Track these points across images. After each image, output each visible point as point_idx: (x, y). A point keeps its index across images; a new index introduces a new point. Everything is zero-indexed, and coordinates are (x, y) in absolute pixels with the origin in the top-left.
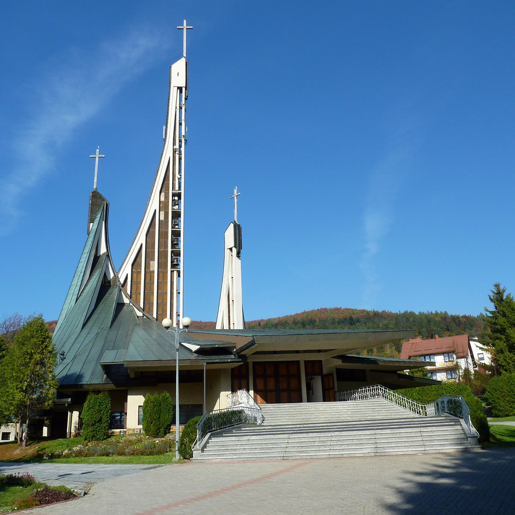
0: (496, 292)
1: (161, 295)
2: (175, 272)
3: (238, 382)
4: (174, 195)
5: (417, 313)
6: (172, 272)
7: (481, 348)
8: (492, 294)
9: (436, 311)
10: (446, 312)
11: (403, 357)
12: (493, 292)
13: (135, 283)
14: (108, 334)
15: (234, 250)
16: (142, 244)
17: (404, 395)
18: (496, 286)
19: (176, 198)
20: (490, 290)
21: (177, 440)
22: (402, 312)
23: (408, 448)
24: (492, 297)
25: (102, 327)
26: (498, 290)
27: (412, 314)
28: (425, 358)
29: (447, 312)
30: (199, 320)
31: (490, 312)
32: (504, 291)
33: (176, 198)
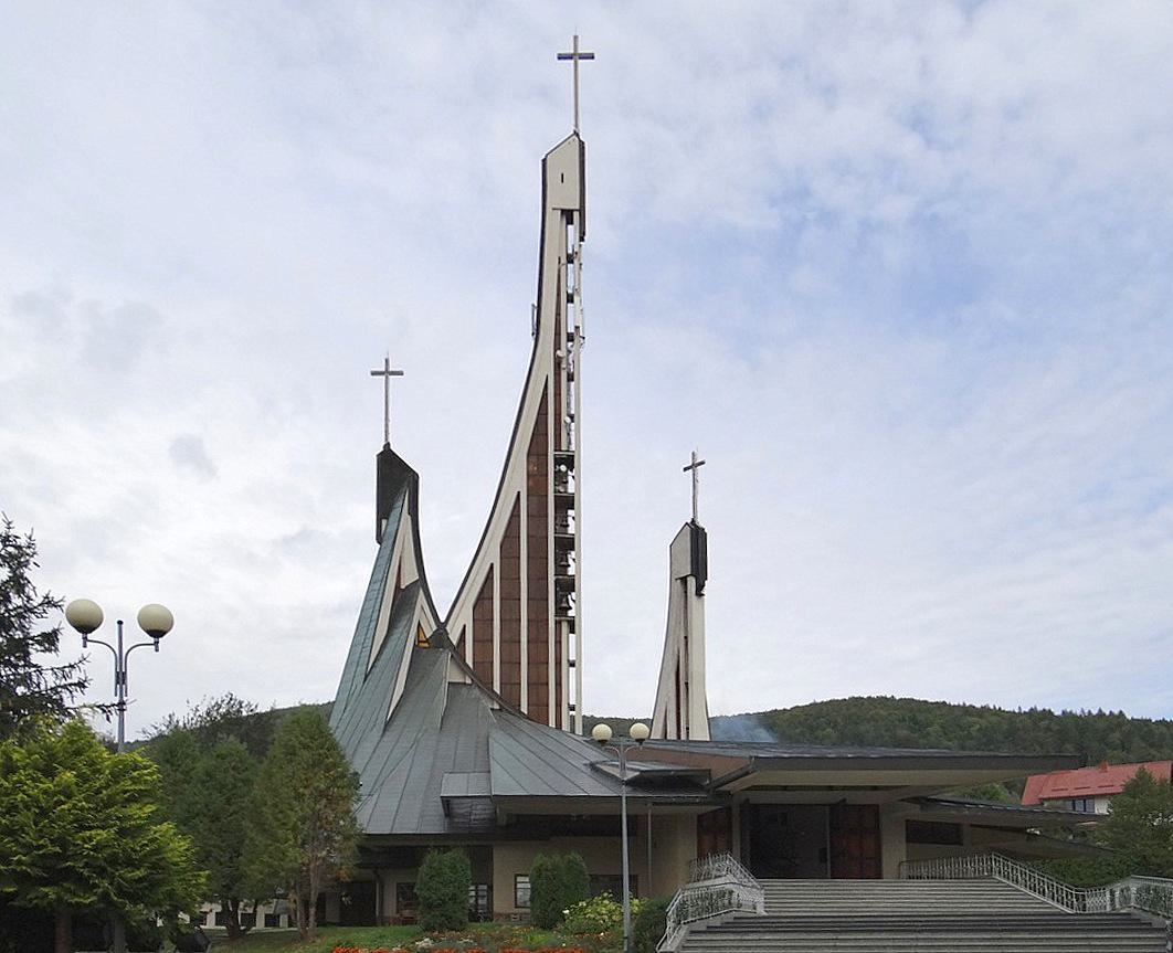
4: (558, 461)
5: (1058, 713)
9: (1100, 710)
11: (1028, 799)
13: (483, 641)
14: (438, 741)
15: (692, 582)
16: (492, 565)
19: (563, 468)
25: (424, 727)
27: (1047, 714)
28: (1074, 803)
29: (1125, 712)
33: (563, 468)
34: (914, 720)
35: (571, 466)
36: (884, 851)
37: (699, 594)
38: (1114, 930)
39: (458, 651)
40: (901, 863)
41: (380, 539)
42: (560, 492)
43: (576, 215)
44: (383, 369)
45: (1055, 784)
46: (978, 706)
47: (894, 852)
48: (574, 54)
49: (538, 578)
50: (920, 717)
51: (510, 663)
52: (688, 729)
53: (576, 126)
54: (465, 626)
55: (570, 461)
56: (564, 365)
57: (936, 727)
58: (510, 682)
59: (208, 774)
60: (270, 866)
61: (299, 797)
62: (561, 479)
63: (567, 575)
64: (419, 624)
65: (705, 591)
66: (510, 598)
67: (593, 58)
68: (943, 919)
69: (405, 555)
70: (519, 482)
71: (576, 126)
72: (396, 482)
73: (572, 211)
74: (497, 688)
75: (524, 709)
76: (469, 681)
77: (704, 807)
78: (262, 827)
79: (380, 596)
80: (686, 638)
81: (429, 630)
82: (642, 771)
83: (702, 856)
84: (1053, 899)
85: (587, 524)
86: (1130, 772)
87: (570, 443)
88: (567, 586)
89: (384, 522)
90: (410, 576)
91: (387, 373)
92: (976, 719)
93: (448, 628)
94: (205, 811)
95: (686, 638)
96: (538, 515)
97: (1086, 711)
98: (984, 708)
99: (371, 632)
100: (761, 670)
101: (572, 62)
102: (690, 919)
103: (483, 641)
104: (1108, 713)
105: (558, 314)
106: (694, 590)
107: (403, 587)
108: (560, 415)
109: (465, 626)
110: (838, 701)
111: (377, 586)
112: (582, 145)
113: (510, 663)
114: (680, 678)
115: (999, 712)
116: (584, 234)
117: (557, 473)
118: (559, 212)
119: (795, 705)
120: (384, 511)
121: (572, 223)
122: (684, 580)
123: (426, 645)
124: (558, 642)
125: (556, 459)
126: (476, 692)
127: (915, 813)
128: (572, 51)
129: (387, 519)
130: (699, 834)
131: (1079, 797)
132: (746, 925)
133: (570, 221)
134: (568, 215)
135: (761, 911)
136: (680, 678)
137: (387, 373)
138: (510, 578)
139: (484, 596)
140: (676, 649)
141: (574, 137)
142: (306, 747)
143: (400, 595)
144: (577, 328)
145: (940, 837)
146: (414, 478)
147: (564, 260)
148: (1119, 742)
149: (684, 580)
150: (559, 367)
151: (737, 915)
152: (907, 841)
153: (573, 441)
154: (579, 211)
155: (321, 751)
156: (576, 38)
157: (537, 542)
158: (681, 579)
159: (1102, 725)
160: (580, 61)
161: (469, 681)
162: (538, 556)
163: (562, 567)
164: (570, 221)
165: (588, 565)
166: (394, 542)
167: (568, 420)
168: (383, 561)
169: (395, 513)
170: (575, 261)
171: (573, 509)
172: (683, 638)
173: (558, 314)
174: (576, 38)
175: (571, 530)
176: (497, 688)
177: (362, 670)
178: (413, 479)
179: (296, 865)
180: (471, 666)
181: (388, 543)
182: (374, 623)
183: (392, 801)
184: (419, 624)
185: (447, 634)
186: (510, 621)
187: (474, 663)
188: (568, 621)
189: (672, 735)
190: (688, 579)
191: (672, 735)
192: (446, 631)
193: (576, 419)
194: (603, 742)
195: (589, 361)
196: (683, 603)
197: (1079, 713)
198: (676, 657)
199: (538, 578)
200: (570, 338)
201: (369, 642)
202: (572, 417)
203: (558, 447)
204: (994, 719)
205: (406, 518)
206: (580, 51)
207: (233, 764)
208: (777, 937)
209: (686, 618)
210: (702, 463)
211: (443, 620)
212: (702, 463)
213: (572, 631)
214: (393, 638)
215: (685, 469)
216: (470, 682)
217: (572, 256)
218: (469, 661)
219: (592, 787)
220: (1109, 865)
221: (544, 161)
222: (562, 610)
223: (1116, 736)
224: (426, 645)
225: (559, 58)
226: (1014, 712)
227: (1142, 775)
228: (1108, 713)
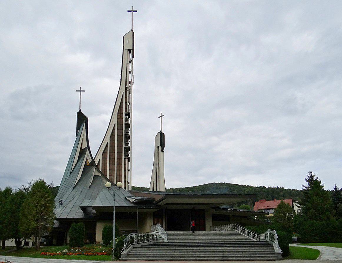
0: (309, 176)
2: (127, 160)
3: (157, 218)
4: (126, 115)
5: (267, 187)
7: (298, 207)
8: (307, 178)
9: (278, 187)
10: (283, 187)
11: (255, 209)
12: (308, 176)
13: (104, 164)
15: (160, 148)
16: (107, 143)
17: (248, 229)
18: (310, 172)
19: (127, 117)
20: (306, 175)
21: (113, 248)
22: (259, 186)
23: (241, 257)
24: (307, 179)
25: (85, 188)
26: (311, 174)
27: (264, 187)
28: (267, 210)
30: (146, 187)
31: (306, 187)
32: (314, 176)
34: (230, 189)
35: (129, 117)
36: (206, 223)
37: (162, 151)
38: (266, 246)
39: (97, 167)
41: (77, 135)
42: (126, 123)
43: (132, 51)
44: (80, 90)
45: (262, 205)
46: (247, 185)
47: (209, 224)
49: (120, 146)
50: (232, 188)
51: (112, 170)
52: (159, 189)
53: (132, 28)
55: (129, 115)
56: (128, 90)
57: (236, 191)
59: (12, 200)
60: (26, 227)
61: (36, 207)
62: (127, 120)
63: (128, 146)
64: (87, 159)
65: (164, 150)
66: (112, 152)
67: (137, 12)
68: (215, 243)
69: (84, 140)
70: (115, 121)
71: (132, 28)
72: (82, 120)
73: (131, 50)
77: (155, 210)
78: (24, 215)
79: (76, 151)
80: (159, 163)
81: (90, 160)
82: (135, 199)
83: (154, 224)
84: (254, 238)
85: (134, 133)
86: (279, 202)
87: (129, 110)
88: (128, 149)
89: (78, 131)
90: (85, 146)
91: (81, 91)
92: (246, 189)
93: (95, 160)
94: (10, 211)
95: (159, 163)
96: (120, 129)
97: (274, 187)
98: (248, 186)
99: (73, 161)
101: (131, 12)
102: (134, 243)
103: (104, 164)
104: (280, 187)
105: (126, 76)
106: (161, 150)
107: (83, 149)
108: (127, 103)
110: (210, 184)
111: (75, 148)
112: (133, 34)
114: (157, 175)
115: (252, 187)
116: (134, 56)
117: (126, 118)
120: (78, 128)
121: (130, 53)
122: (158, 147)
123: (89, 165)
124: (125, 164)
125: (125, 114)
126: (102, 178)
127: (214, 211)
128: (131, 10)
129: (79, 130)
130: (153, 218)
131: (268, 209)
132: (161, 245)
133: (130, 53)
134: (129, 51)
135: (166, 240)
136: (157, 175)
138: (112, 147)
139: (105, 152)
141: (131, 31)
142: (38, 191)
143: (83, 151)
144: (131, 80)
145: (222, 219)
146: (87, 119)
147: (128, 62)
148: (282, 195)
149: (158, 147)
150: (127, 89)
151: (155, 242)
153: (130, 110)
154: (132, 50)
155: (43, 193)
156: (132, 6)
157: (120, 136)
159: (278, 190)
160: (133, 12)
161: (100, 175)
162: (120, 141)
163: (126, 144)
164: (130, 53)
165: (133, 143)
166: (80, 136)
167: (129, 104)
169: (81, 128)
170: (131, 63)
171: (130, 128)
172: (158, 163)
173: (126, 76)
174: (132, 6)
175: (129, 134)
176: (108, 177)
177: (69, 172)
178: (86, 120)
179: (34, 227)
180: (101, 171)
181: (79, 136)
182: (74, 158)
183: (67, 209)
184: (87, 159)
187: (102, 170)
189: (155, 190)
190: (160, 147)
191: (155, 190)
193: (131, 103)
194: (108, 188)
197: (272, 187)
199: (120, 146)
200: (130, 83)
201: (72, 163)
202: (130, 103)
203: (126, 111)
204: (250, 189)
205: (84, 130)
206: (133, 10)
207: (20, 197)
208: (162, 249)
210: (163, 116)
211: (94, 158)
212: (163, 116)
213: (129, 161)
214: (78, 163)
215: (159, 117)
216: (101, 175)
217: (130, 61)
218: (100, 169)
219: (125, 204)
220: (274, 228)
221: (124, 37)
222: (126, 156)
223: (282, 193)
224: (89, 165)
225: (128, 11)
226: (256, 187)
227: (282, 203)
228: (280, 187)
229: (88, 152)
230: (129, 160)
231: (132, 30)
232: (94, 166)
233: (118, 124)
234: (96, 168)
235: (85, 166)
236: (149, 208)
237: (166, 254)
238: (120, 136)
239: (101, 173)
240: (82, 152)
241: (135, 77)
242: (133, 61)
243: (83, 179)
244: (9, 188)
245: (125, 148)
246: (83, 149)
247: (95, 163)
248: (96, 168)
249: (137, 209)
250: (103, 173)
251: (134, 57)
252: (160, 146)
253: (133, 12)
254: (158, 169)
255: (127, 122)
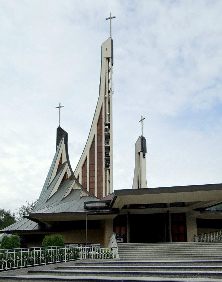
1: (100, 182)
4: (106, 125)
6: (106, 170)
13: (84, 177)
15: (142, 154)
33: (107, 127)
36: (187, 231)
37: (144, 156)
40: (195, 236)
43: (110, 59)
44: (59, 106)
47: (192, 231)
48: (110, 17)
49: (100, 158)
51: (92, 183)
54: (79, 173)
55: (109, 125)
58: (92, 188)
66: (92, 164)
70: (95, 132)
71: (111, 35)
72: (61, 135)
74: (88, 190)
75: (96, 195)
76: (145, 207)
80: (140, 170)
81: (69, 174)
89: (58, 146)
91: (60, 107)
93: (74, 174)
95: (140, 170)
96: (100, 141)
99: (51, 175)
100: (159, 177)
103: (84, 177)
109: (79, 173)
113: (92, 183)
117: (106, 129)
118: (106, 59)
119: (68, 133)
120: (58, 144)
122: (139, 153)
127: (198, 214)
134: (108, 59)
137: (60, 107)
138: (92, 159)
139: (85, 165)
140: (138, 174)
143: (61, 164)
147: (107, 71)
149: (139, 153)
152: (198, 227)
157: (100, 148)
158: (138, 153)
161: (80, 188)
162: (100, 153)
164: (109, 61)
168: (56, 156)
176: (88, 190)
178: (66, 135)
185: (74, 175)
186: (92, 171)
188: (109, 170)
190: (140, 153)
192: (74, 175)
195: (115, 98)
196: (139, 160)
198: (137, 177)
203: (105, 121)
209: (140, 164)
218: (80, 182)
221: (102, 46)
222: (107, 166)
224: (69, 179)
229: (67, 165)
230: (109, 170)
231: (111, 38)
232: (73, 179)
233: (98, 136)
234: (76, 182)
235: (64, 179)
236: (102, 213)
237: (215, 251)
238: (100, 148)
239: (81, 186)
240: (61, 167)
241: (115, 85)
242: (112, 70)
243: (59, 192)
244: (27, 210)
245: (105, 159)
246: (62, 163)
247: (75, 176)
248: (76, 181)
249: (87, 215)
250: (83, 186)
251: (113, 65)
252: (141, 151)
253: (112, 18)
254: (139, 177)
255: (107, 133)
